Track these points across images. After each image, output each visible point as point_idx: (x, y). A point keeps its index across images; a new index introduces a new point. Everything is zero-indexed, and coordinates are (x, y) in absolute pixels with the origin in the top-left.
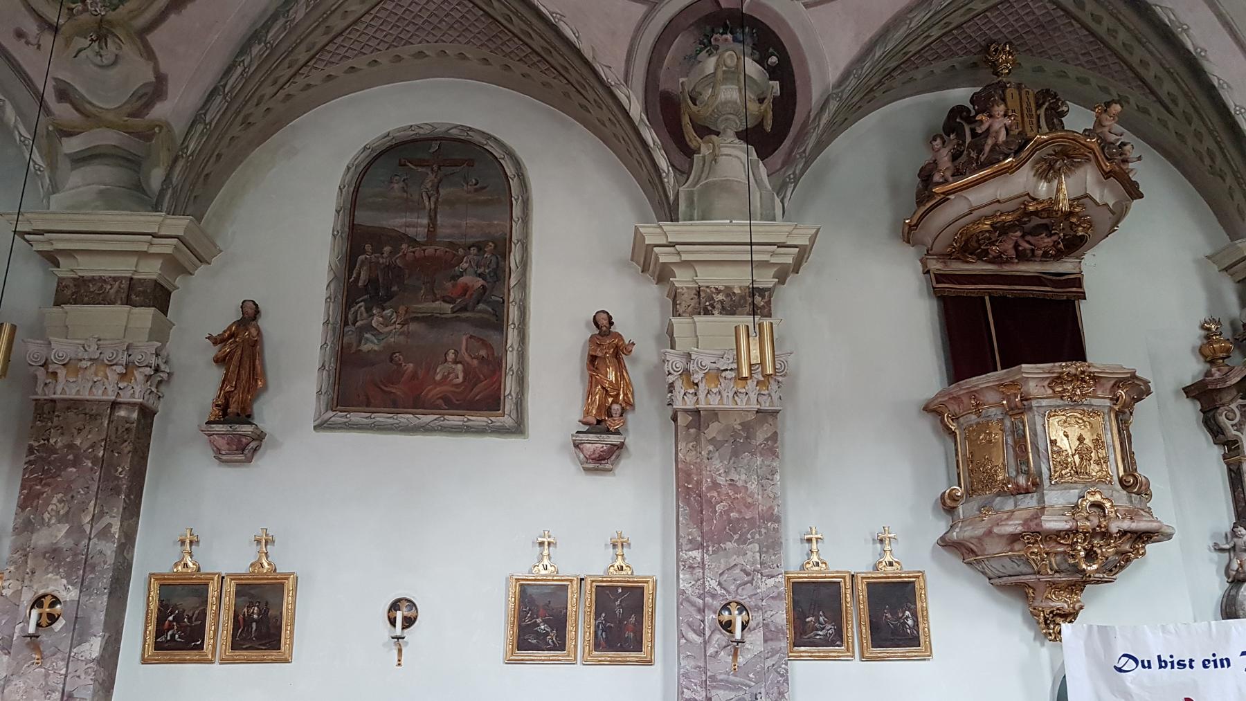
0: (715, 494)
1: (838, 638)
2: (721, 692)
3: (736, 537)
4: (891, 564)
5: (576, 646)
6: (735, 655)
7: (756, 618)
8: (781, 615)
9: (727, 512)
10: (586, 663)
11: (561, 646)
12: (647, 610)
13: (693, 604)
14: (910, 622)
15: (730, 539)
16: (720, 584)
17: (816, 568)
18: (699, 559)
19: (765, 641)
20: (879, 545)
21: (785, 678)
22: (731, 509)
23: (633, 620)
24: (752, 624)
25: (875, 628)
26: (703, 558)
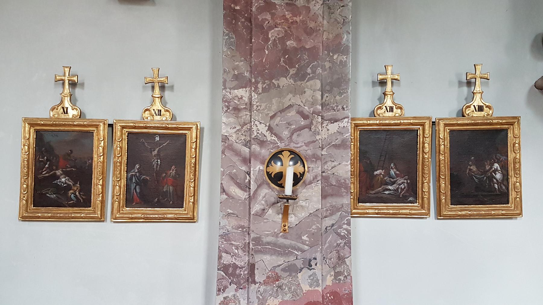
0: (268, 17)
1: (411, 193)
2: (267, 258)
3: (292, 71)
4: (481, 109)
5: (103, 202)
6: (285, 213)
7: (313, 170)
8: (344, 167)
9: (283, 40)
10: (115, 219)
11: (86, 202)
12: (189, 160)
13: (237, 153)
14: (498, 176)
15: (285, 73)
16: (270, 129)
17: (390, 114)
18: (246, 99)
19: (324, 196)
20: (465, 89)
21: (347, 240)
22: (287, 36)
23: (173, 172)
24: (308, 177)
25: (456, 182)
26: (250, 99)
